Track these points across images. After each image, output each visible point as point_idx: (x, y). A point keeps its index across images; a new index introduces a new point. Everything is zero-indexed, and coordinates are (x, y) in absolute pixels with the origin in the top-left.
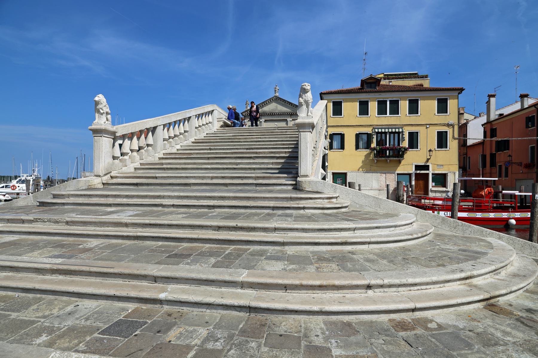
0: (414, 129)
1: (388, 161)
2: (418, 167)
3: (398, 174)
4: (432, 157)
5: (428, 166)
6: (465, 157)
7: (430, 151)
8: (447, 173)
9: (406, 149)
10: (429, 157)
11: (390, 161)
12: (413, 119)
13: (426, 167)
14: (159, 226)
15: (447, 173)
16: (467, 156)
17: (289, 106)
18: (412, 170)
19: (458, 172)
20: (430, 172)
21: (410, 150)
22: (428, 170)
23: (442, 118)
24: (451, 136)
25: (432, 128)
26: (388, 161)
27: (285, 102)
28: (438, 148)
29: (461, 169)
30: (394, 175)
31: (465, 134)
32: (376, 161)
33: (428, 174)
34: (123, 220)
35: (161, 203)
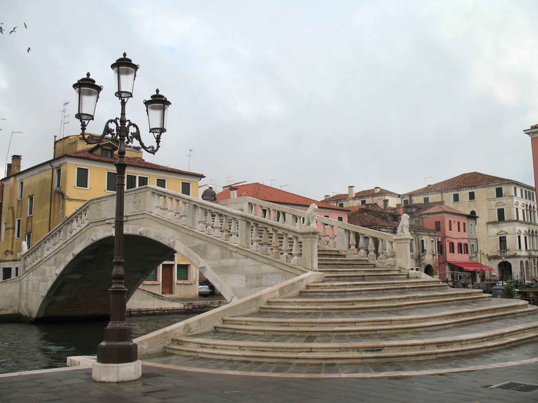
8: (190, 264)
33: (172, 265)
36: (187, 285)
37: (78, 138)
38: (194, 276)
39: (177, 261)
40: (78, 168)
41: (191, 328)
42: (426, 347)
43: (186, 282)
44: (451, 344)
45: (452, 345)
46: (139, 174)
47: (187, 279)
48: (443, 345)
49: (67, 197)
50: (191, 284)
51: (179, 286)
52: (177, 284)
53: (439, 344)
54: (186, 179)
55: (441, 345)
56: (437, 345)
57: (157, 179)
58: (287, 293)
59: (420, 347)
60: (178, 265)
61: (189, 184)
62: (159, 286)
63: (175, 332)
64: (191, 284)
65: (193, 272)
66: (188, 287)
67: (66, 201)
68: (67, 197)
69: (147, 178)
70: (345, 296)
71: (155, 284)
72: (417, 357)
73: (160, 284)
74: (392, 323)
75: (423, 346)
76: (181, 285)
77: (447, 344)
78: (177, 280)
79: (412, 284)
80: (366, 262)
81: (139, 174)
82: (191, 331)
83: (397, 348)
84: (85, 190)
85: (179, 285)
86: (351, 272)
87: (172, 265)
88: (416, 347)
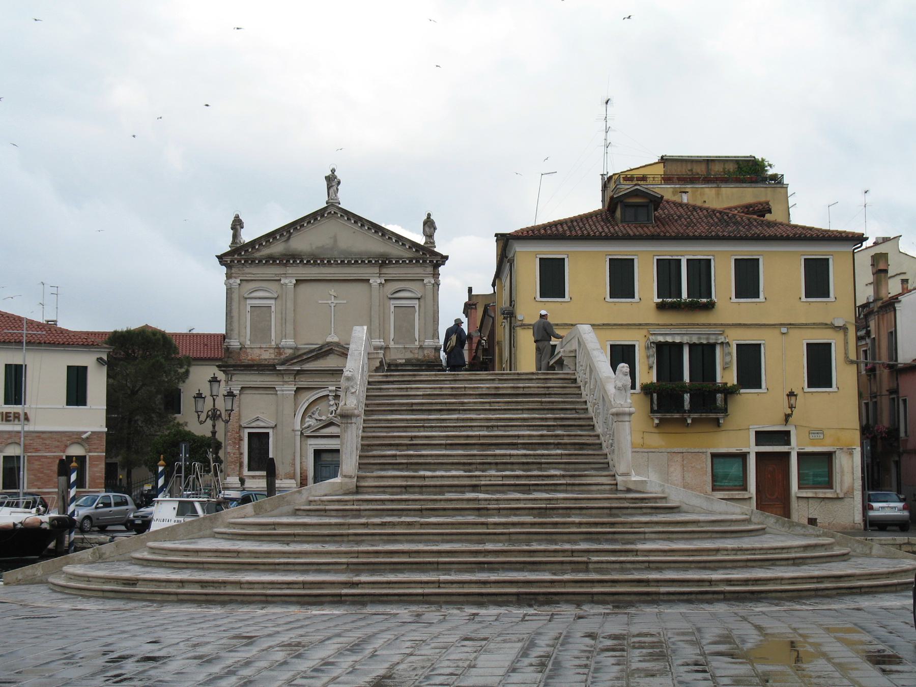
0: (749, 337)
1: (689, 421)
2: (762, 437)
3: (714, 456)
4: (795, 411)
5: (788, 433)
6: (893, 399)
7: (791, 394)
8: (835, 452)
9: (729, 392)
10: (789, 411)
11: (693, 420)
12: (746, 309)
13: (783, 437)
14: (662, 525)
15: (835, 452)
16: (898, 398)
17: (375, 236)
18: (753, 449)
19: (859, 449)
20: (795, 448)
21: (742, 391)
22: (788, 443)
23: (816, 309)
24: (841, 357)
25: (794, 333)
26: (689, 421)
27: (362, 225)
28: (809, 386)
29: (869, 441)
30: (704, 456)
31: (891, 333)
32: (657, 421)
33: (788, 454)
34: (112, 607)
35: (143, 570)
36: (827, 501)
37: (621, 179)
38: (847, 480)
39: (797, 446)
40: (540, 259)
41: (104, 554)
42: (186, 585)
43: (829, 493)
44: (222, 585)
45: (225, 587)
46: (687, 253)
47: (829, 485)
48: (209, 586)
49: (520, 323)
50: (838, 498)
51: (803, 503)
52: (798, 498)
53: (204, 584)
54: (816, 251)
55: (206, 584)
56: (201, 584)
57: (735, 260)
58: (269, 510)
59: (176, 584)
60: (799, 454)
61: (828, 259)
62: (748, 501)
63: (80, 557)
64: (838, 498)
65: (842, 472)
66: (837, 505)
67: (518, 329)
68: (520, 323)
69: (710, 260)
70: (359, 517)
71: (737, 497)
72: (152, 595)
73: (750, 498)
74: (240, 555)
75: (181, 585)
76: (811, 501)
77: (216, 585)
78: (799, 488)
79: (533, 502)
80: (602, 457)
81: (687, 253)
82: (104, 556)
83: (151, 583)
84: (559, 304)
85: (805, 501)
86: (415, 479)
87: (758, 454)
88: (172, 584)
